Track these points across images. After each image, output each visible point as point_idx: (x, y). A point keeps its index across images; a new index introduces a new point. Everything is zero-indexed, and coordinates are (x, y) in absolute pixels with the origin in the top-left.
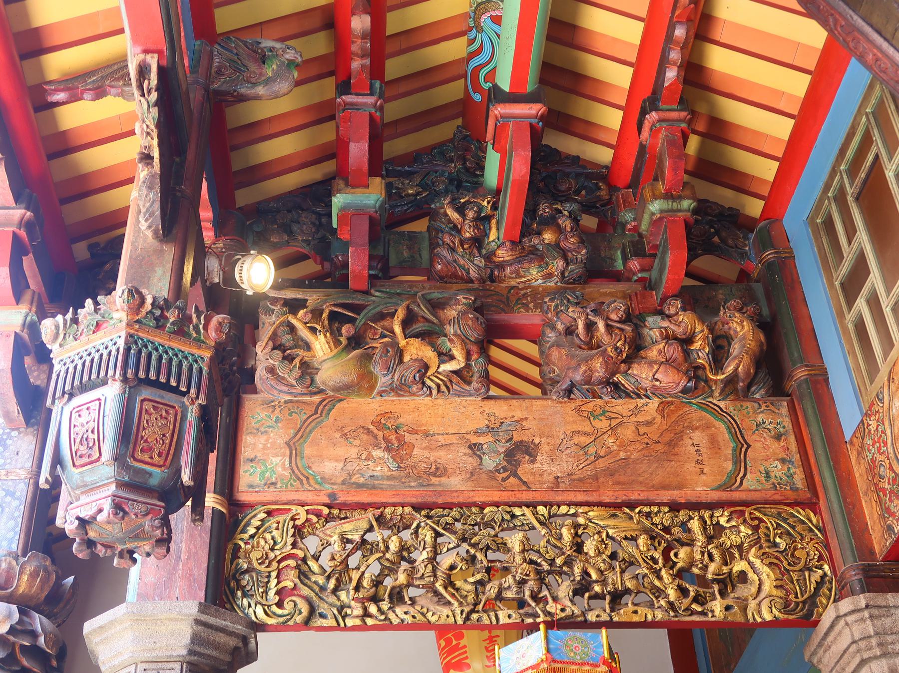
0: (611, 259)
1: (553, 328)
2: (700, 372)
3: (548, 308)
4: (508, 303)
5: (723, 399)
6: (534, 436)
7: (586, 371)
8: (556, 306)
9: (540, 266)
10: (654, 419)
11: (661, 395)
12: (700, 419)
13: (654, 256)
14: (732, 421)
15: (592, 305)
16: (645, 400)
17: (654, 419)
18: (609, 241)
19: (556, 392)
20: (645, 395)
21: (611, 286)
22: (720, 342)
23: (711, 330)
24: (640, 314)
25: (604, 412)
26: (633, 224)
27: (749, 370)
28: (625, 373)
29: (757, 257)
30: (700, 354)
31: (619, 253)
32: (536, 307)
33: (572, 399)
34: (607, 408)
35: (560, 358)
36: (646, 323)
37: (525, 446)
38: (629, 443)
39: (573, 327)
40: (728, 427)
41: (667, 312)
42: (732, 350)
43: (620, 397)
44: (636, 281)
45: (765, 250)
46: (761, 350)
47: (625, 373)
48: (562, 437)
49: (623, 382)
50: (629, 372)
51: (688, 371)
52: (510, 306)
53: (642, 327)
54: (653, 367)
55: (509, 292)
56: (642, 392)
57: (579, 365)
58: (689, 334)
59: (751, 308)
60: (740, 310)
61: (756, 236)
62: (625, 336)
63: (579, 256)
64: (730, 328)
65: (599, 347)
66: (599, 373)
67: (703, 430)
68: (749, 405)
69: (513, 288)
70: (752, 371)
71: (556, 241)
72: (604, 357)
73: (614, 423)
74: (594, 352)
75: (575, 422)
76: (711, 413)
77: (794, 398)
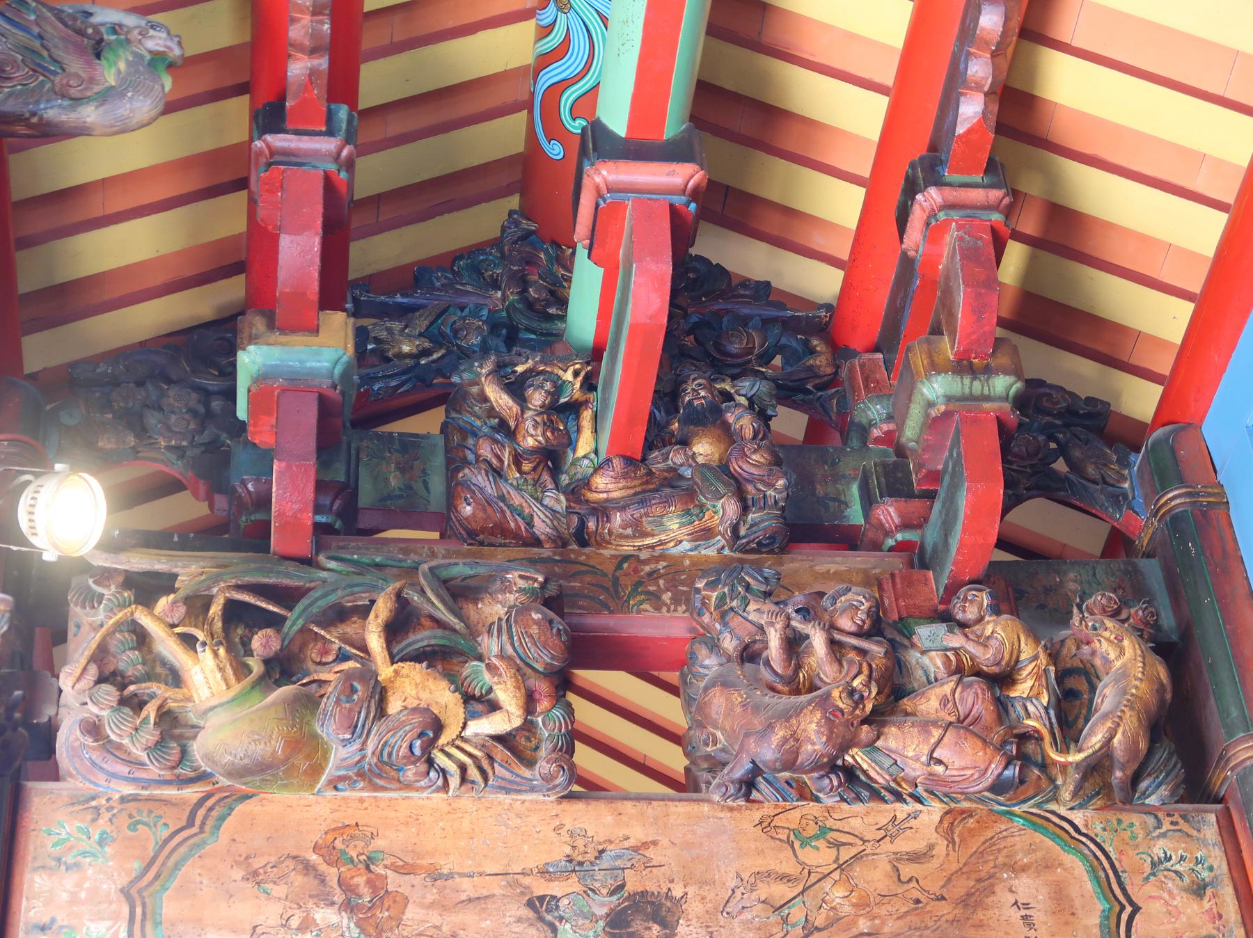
2: (1030, 747)
3: (704, 604)
4: (617, 592)
5: (1081, 806)
6: (672, 881)
7: (785, 740)
8: (722, 599)
9: (687, 512)
10: (931, 847)
11: (946, 795)
12: (1031, 849)
13: (931, 496)
14: (1099, 853)
15: (799, 599)
16: (913, 806)
17: (931, 847)
18: (833, 464)
19: (719, 786)
20: (912, 796)
21: (838, 559)
22: (1072, 683)
23: (1054, 657)
24: (901, 619)
25: (824, 831)
26: (885, 427)
27: (1136, 743)
28: (870, 746)
29: (1147, 503)
30: (1031, 708)
31: (855, 489)
32: (676, 601)
33: (754, 801)
34: (830, 823)
35: (729, 712)
36: (915, 639)
37: (652, 903)
38: (878, 899)
39: (758, 646)
40: (1091, 866)
41: (960, 616)
42: (1097, 700)
43: (859, 798)
44: (891, 549)
45: (1165, 486)
46: (1162, 701)
48: (732, 883)
49: (865, 766)
50: (879, 744)
51: (1004, 743)
52: (620, 598)
53: (906, 647)
54: (929, 733)
55: (619, 567)
56: (906, 789)
57: (770, 727)
58: (1008, 664)
59: (1137, 612)
60: (1115, 615)
62: (870, 666)
63: (771, 493)
64: (1094, 653)
65: (812, 688)
66: (813, 744)
67: (1038, 872)
68: (1135, 819)
69: (626, 558)
70: (1143, 745)
71: (720, 460)
72: (824, 711)
73: (846, 854)
74: (803, 698)
75: (760, 853)
76: (1054, 837)
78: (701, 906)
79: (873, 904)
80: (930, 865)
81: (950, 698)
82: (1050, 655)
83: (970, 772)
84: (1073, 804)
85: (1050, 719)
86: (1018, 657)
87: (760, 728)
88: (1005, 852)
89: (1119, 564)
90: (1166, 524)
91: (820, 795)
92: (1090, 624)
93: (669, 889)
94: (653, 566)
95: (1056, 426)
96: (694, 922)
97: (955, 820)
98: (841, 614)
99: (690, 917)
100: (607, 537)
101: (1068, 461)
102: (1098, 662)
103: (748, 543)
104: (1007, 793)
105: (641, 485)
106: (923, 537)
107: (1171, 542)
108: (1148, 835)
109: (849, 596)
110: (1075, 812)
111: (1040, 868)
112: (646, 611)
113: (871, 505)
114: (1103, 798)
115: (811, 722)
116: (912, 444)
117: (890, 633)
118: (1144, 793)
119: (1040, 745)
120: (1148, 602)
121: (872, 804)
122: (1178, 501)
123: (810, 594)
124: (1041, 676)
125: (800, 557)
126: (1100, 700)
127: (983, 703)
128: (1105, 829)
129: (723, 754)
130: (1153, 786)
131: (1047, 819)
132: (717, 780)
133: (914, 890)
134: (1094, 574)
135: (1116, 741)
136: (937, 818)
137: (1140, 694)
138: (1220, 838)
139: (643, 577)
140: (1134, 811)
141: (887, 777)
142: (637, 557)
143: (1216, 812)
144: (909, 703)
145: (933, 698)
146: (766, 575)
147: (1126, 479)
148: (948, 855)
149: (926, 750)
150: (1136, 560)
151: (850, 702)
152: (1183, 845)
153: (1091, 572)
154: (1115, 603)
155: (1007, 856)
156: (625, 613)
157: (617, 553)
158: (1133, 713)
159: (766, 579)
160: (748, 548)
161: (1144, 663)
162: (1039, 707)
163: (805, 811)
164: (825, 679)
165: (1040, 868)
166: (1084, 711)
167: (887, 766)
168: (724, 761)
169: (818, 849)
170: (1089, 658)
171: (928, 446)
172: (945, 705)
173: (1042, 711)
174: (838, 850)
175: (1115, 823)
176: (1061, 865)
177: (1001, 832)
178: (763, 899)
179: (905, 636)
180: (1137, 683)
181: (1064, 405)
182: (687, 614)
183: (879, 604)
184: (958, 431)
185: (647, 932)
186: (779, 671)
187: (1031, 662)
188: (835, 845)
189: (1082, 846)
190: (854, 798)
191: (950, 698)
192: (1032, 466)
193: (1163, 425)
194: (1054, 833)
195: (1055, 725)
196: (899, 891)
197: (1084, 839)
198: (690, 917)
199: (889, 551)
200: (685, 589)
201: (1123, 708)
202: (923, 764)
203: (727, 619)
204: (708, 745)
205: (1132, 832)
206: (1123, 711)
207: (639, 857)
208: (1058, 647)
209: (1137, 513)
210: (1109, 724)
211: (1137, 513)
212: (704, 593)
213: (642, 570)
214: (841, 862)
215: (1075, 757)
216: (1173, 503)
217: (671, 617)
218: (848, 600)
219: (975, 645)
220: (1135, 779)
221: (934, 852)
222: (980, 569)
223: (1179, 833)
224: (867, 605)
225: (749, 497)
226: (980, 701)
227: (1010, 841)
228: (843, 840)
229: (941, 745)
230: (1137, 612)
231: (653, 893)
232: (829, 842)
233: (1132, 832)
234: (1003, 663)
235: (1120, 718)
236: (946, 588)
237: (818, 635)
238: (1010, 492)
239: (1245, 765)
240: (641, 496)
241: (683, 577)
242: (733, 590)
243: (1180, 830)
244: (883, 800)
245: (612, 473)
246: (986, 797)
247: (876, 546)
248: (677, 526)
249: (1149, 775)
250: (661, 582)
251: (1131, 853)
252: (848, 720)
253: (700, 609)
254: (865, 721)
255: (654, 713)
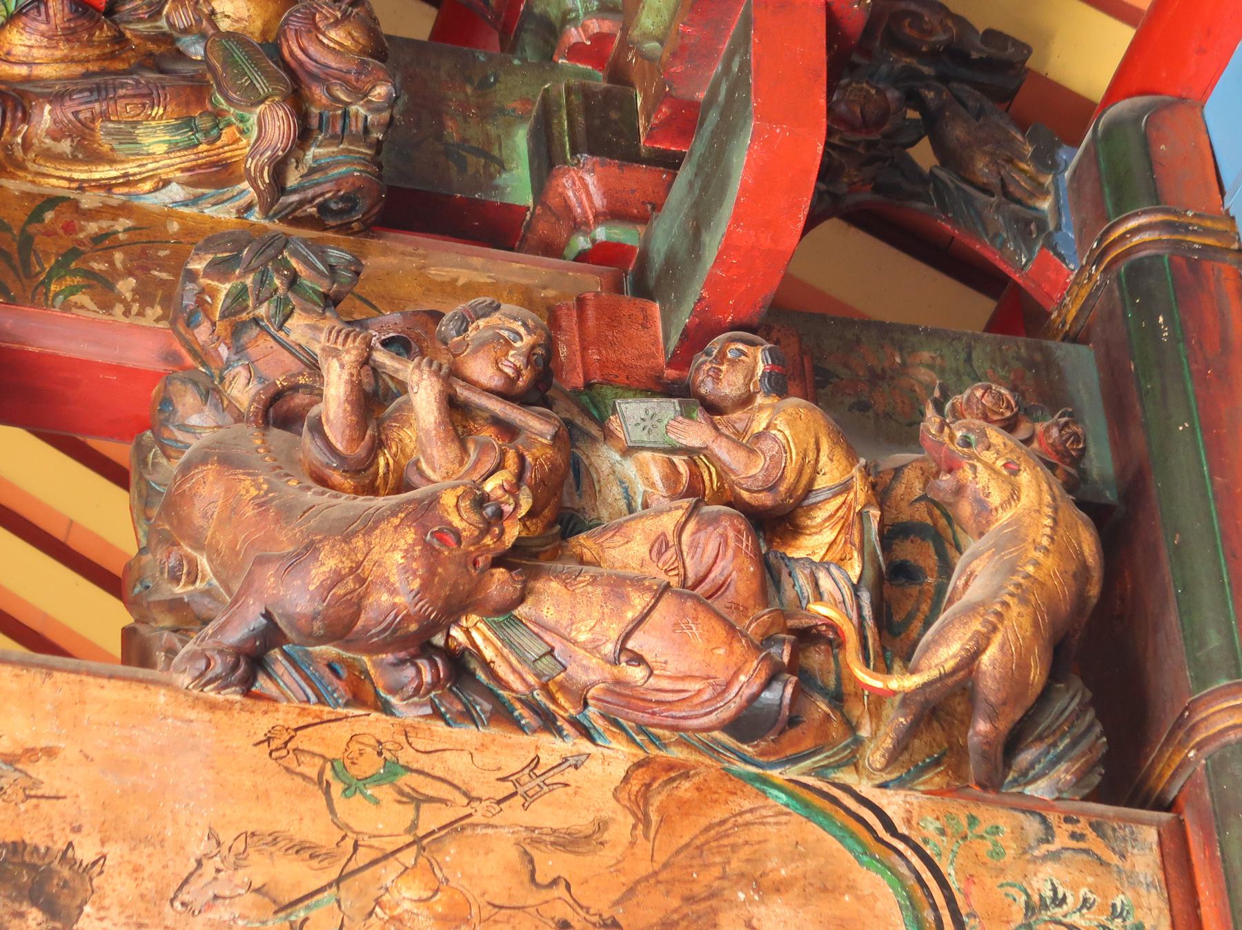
0: (484, 153)
1: (211, 392)
2: (816, 658)
3: (201, 303)
4: (26, 264)
5: (901, 783)
6: (77, 830)
7: (337, 578)
8: (239, 296)
9: (187, 123)
10: (602, 825)
11: (641, 729)
12: (797, 852)
13: (671, 163)
14: (927, 876)
15: (391, 321)
16: (573, 744)
17: (602, 825)
18: (484, 86)
19: (193, 657)
20: (574, 723)
21: (477, 261)
22: (908, 551)
23: (881, 493)
24: (589, 386)
25: (393, 769)
26: (595, 26)
27: (1024, 667)
28: (504, 612)
29: (1083, 239)
30: (825, 583)
31: (521, 139)
32: (144, 296)
33: (260, 697)
34: (406, 756)
35: (232, 512)
36: (614, 423)
37: (33, 868)
38: (487, 911)
39: (300, 399)
40: (910, 898)
41: (707, 388)
42: (956, 581)
43: (468, 716)
44: (582, 257)
45: (1123, 207)
46: (1080, 598)
47: (504, 612)
48: (198, 847)
49: (489, 654)
50: (522, 611)
51: (768, 640)
52: (30, 276)
53: (594, 440)
54: (624, 599)
55: (36, 216)
56: (566, 708)
57: (309, 549)
58: (791, 492)
59: (1049, 429)
60: (1009, 426)
61: (1091, 155)
62: (522, 458)
63: (358, 109)
64: (959, 490)
65: (402, 486)
66: (393, 592)
67: (806, 897)
68: (1005, 820)
69: (52, 202)
70: (1036, 675)
71: (264, 33)
72: (423, 529)
73: (432, 819)
74: (382, 502)
75: (261, 796)
76: (843, 835)
77: (1188, 817)
78: (130, 884)
79: (475, 920)
80: (596, 858)
81: (672, 539)
82: (873, 486)
83: (695, 686)
84: (886, 777)
85: (859, 608)
86: (812, 481)
87: (291, 549)
88: (745, 852)
89: (1017, 346)
90: (1118, 277)
91: (394, 700)
92: (959, 434)
93: (70, 845)
94: (105, 224)
95: (920, 76)
96: (114, 912)
97: (654, 779)
98: (475, 351)
99: (106, 902)
100: (19, 153)
101: (940, 147)
102: (965, 509)
103: (301, 203)
104: (762, 737)
105: (100, 58)
106: (647, 240)
107: (1125, 315)
108: (1025, 852)
109: (495, 319)
110: (890, 792)
111: (809, 889)
112: (82, 307)
113: (551, 165)
114: (945, 772)
115: (394, 548)
116: (652, 46)
117: (565, 409)
118: (1024, 774)
119: (836, 657)
120: (1070, 415)
121: (494, 731)
122: (1146, 236)
123: (415, 313)
124: (851, 525)
125: (400, 247)
126: (961, 583)
127: (735, 556)
128: (942, 832)
129: (206, 601)
130: (1044, 761)
131: (835, 801)
132: (190, 646)
133: (559, 903)
134: (969, 359)
135: (985, 659)
136: (620, 772)
137: (1041, 576)
138: (1161, 875)
139: (81, 242)
140: (1003, 805)
141: (531, 679)
142: (75, 204)
143: (1158, 825)
144: (589, 543)
145: (638, 537)
146: (332, 261)
147: (1047, 193)
148: (633, 844)
149: (614, 631)
150: (1050, 343)
151: (475, 518)
152: (1090, 880)
153: (963, 356)
154: (1009, 407)
155: (748, 861)
156: (39, 306)
157: (35, 189)
158: (1023, 610)
159: (331, 268)
160: (298, 213)
161: (1055, 521)
162: (842, 583)
163: (360, 727)
164: (429, 472)
165: (809, 889)
166: (925, 607)
167: (532, 655)
168: (205, 613)
169: (377, 802)
170: (949, 499)
171: (683, 48)
172: (660, 554)
173: (847, 592)
174: (418, 809)
175: (964, 822)
176: (851, 888)
177: (741, 814)
178: (256, 885)
179: (592, 418)
180: (1039, 555)
181: (943, 37)
182: (163, 325)
183: (550, 346)
184: (747, 21)
185: (16, 922)
186: (339, 447)
187: (835, 495)
188: (413, 799)
189: (896, 859)
190: (461, 714)
191: (672, 539)
192: (870, 145)
193: (1130, 95)
194: (843, 828)
195: (870, 622)
196: (531, 901)
197: (901, 846)
198: (106, 902)
199: (576, 259)
200: (164, 276)
201: (1008, 599)
202: (605, 659)
203: (245, 339)
204: (176, 580)
205: (995, 844)
206: (1005, 604)
207: (17, 775)
208: (888, 478)
209: (1063, 259)
210: (977, 625)
211: (1063, 259)
212: (203, 281)
213: (82, 229)
214: (421, 833)
215: (902, 682)
216: (1136, 240)
217: (131, 325)
218: (493, 328)
219: (731, 446)
220: (1013, 742)
221: (606, 836)
222: (754, 309)
223: (1084, 856)
224: (528, 340)
225: (315, 111)
226: (730, 553)
227: (756, 832)
228: (430, 792)
229: (646, 625)
230: (1048, 429)
231: (36, 849)
232: (401, 792)
233: (995, 844)
234: (783, 488)
235: (999, 615)
236: (686, 333)
237: (425, 383)
238: (823, 187)
239: (1224, 740)
240: (97, 80)
241: (162, 253)
242: (262, 283)
243: (1086, 851)
244: (517, 725)
245: (43, 27)
246: (719, 743)
247: (552, 249)
248: (164, 148)
249: (1040, 738)
250: (118, 256)
251: (989, 881)
252: (468, 554)
253: (192, 313)
254: (499, 561)
255: (46, 616)
